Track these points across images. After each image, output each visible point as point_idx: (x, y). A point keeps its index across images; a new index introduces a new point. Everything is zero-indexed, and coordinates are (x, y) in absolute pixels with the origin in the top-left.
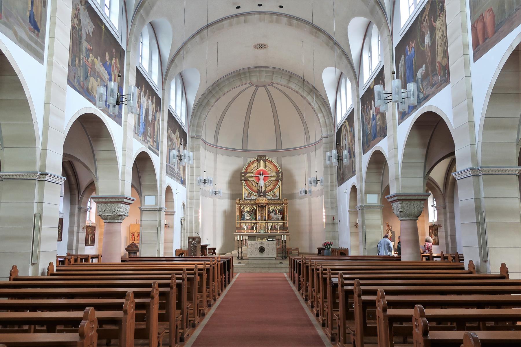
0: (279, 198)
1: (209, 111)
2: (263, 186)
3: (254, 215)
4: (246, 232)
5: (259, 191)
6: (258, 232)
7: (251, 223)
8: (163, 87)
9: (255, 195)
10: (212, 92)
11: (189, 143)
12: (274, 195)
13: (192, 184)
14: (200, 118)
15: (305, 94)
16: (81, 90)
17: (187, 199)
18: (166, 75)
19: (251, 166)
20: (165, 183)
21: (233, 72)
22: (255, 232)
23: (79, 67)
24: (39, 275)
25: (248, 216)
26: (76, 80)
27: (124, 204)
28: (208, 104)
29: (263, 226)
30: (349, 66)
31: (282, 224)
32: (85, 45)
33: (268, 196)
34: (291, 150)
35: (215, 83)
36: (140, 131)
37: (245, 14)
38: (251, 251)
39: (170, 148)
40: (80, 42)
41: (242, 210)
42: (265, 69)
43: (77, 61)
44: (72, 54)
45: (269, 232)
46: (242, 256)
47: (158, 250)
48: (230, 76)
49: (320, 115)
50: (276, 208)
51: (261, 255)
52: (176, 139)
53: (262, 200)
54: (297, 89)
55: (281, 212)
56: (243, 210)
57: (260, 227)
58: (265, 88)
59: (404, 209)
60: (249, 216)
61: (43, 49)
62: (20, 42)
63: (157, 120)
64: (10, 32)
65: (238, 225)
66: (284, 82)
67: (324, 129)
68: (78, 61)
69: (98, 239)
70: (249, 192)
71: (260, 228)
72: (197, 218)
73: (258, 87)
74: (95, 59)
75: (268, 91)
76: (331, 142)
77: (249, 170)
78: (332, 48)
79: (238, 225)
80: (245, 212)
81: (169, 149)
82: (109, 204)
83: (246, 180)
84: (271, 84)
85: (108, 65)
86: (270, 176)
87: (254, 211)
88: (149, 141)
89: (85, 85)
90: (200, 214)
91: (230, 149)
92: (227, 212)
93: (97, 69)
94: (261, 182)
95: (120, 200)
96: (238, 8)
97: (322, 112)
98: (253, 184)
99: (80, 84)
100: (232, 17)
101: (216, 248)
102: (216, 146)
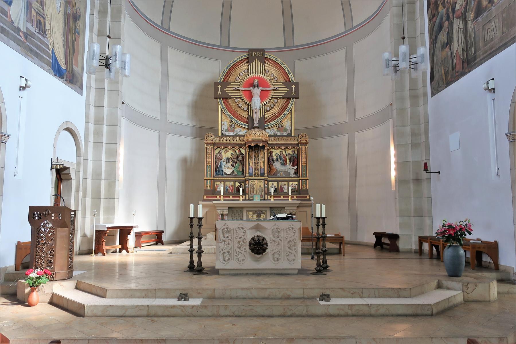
0: (289, 132)
2: (258, 108)
3: (241, 167)
6: (249, 199)
7: (235, 181)
17: (87, 122)
25: (228, 168)
29: (258, 186)
34: (310, 45)
38: (226, 251)
41: (216, 155)
45: (270, 200)
50: (284, 153)
55: (295, 160)
56: (218, 155)
57: (253, 189)
60: (231, 168)
65: (209, 185)
70: (232, 121)
71: (254, 192)
72: (112, 166)
77: (231, 79)
79: (209, 185)
83: (226, 98)
87: (240, 158)
91: (196, 43)
98: (240, 106)
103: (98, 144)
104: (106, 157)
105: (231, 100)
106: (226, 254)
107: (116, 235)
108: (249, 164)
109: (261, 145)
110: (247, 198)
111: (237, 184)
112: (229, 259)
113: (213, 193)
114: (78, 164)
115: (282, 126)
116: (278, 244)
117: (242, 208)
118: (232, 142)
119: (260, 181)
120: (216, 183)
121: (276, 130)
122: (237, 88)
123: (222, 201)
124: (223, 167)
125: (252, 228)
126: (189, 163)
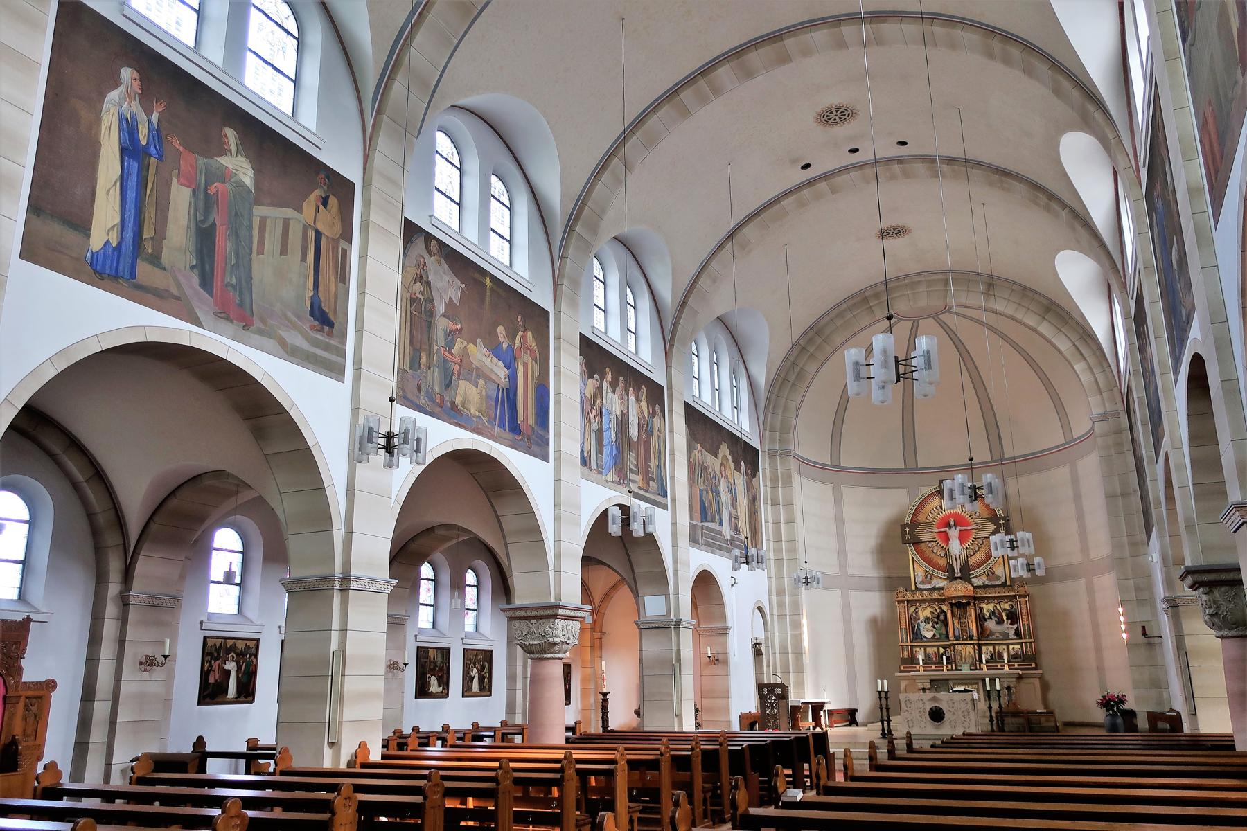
0: (1003, 581)
1: (806, 391)
2: (958, 553)
3: (944, 628)
4: (924, 671)
5: (952, 566)
6: (956, 669)
7: (938, 646)
8: (668, 361)
9: (941, 578)
10: (808, 348)
11: (764, 469)
12: (991, 575)
13: (779, 561)
14: (786, 409)
15: (1031, 320)
16: (437, 410)
17: (770, 595)
18: (673, 337)
19: (925, 506)
20: (689, 566)
21: (850, 298)
22: (948, 670)
23: (429, 369)
24: (343, 766)
26: (422, 393)
27: (562, 619)
28: (800, 376)
29: (967, 653)
30: (1096, 244)
31: (1019, 647)
32: (442, 324)
33: (976, 577)
34: (1028, 458)
35: (811, 327)
36: (604, 463)
37: (826, 176)
38: (909, 719)
39: (703, 487)
40: (431, 322)
41: (912, 615)
42: (923, 279)
43: (424, 359)
44: (412, 349)
45: (919, 671)
46: (890, 731)
47: (679, 716)
48: (844, 306)
49: (1079, 367)
50: (998, 608)
51: (936, 728)
52: (722, 464)
53: (960, 589)
54: (1010, 310)
55: (1013, 617)
56: (914, 615)
57: (961, 656)
58: (934, 319)
59: (1218, 607)
60: (932, 631)
61: (343, 354)
62: (293, 354)
63: (656, 432)
64: (270, 343)
65: (906, 653)
66: (977, 299)
67: (1094, 400)
68: (427, 359)
69: (579, 690)
70: (927, 571)
71: (962, 660)
72: (798, 638)
73: (916, 321)
74: (471, 346)
75: (943, 325)
76: (1118, 432)
77: (921, 518)
78: (1048, 209)
79: (906, 653)
80: (919, 621)
81: (700, 490)
82: (533, 621)
83: (916, 542)
84: (947, 309)
85: (504, 350)
86: (975, 529)
87: (942, 617)
88: (634, 482)
89: (447, 398)
90: (805, 629)
91: (874, 471)
92: (879, 619)
93: (475, 363)
94: (954, 544)
95: (551, 612)
96: (806, 166)
97: (1085, 359)
98: (935, 551)
99: (432, 399)
100: (799, 188)
101: (856, 710)
102: (839, 466)
103: (782, 617)
104: (791, 630)
105: (923, 544)
106: (910, 722)
107: (808, 712)
108: (953, 625)
109: (964, 601)
110: (954, 668)
111: (942, 650)
112: (912, 726)
113: (912, 661)
114: (767, 638)
115: (993, 574)
116: (954, 713)
117: (948, 680)
118: (929, 597)
119: (969, 646)
120: (915, 650)
121: (985, 579)
122: (929, 530)
123: (922, 672)
124: (922, 629)
125: (929, 700)
126: (880, 623)
